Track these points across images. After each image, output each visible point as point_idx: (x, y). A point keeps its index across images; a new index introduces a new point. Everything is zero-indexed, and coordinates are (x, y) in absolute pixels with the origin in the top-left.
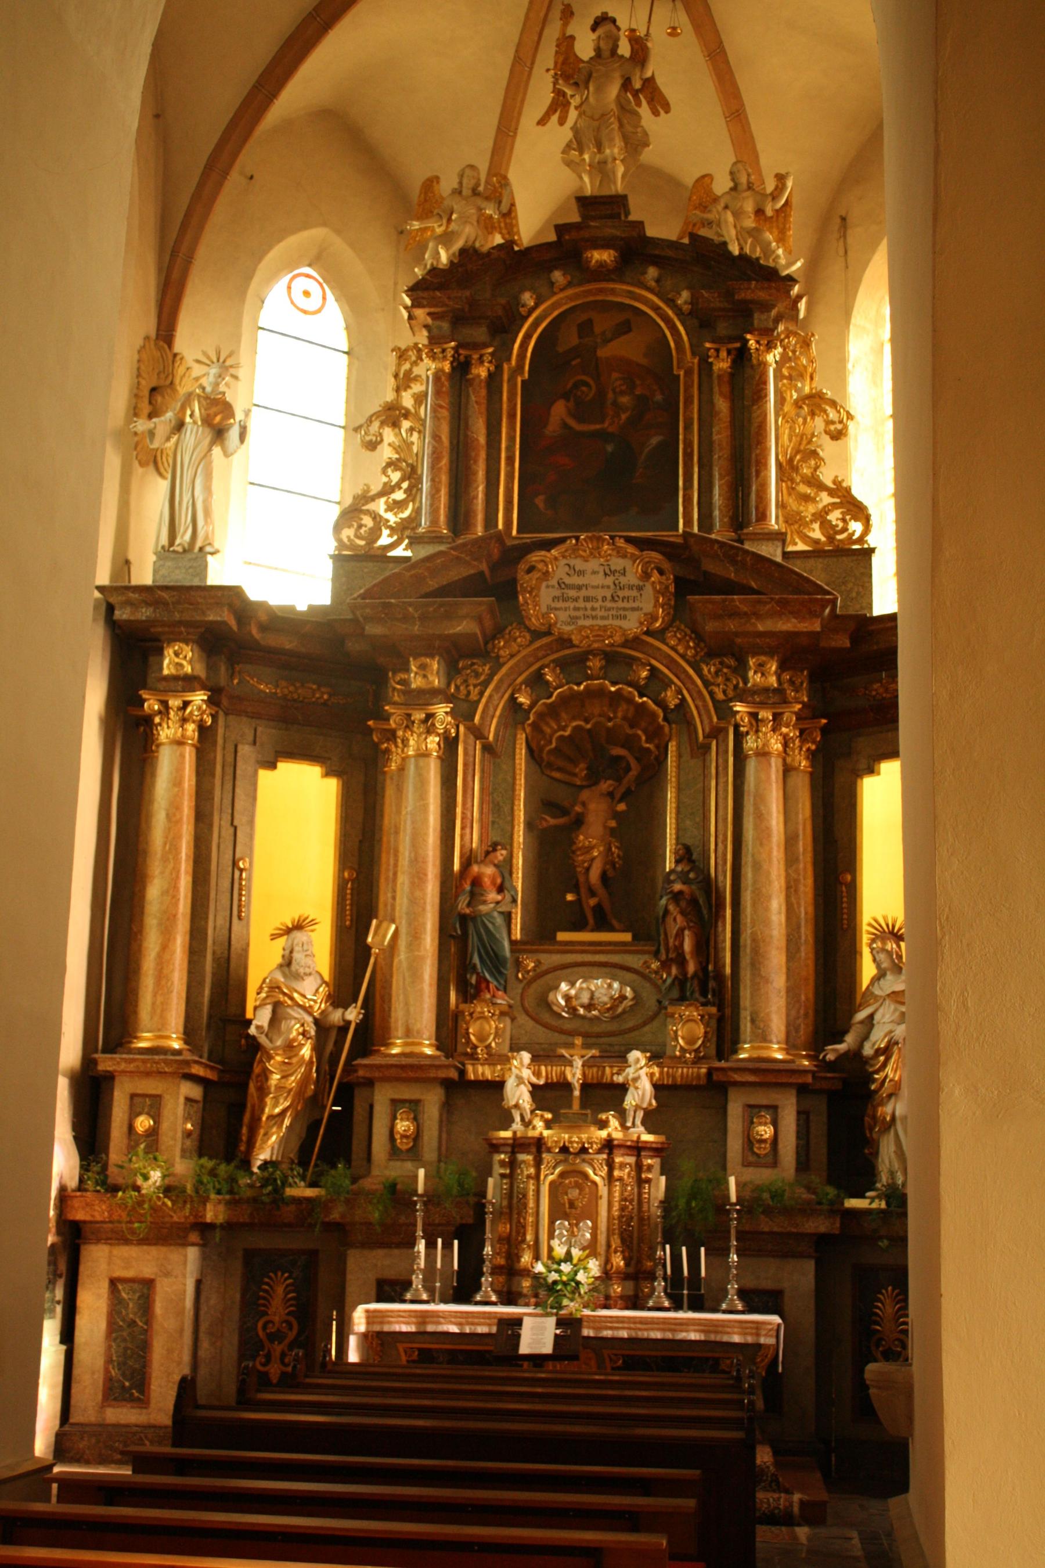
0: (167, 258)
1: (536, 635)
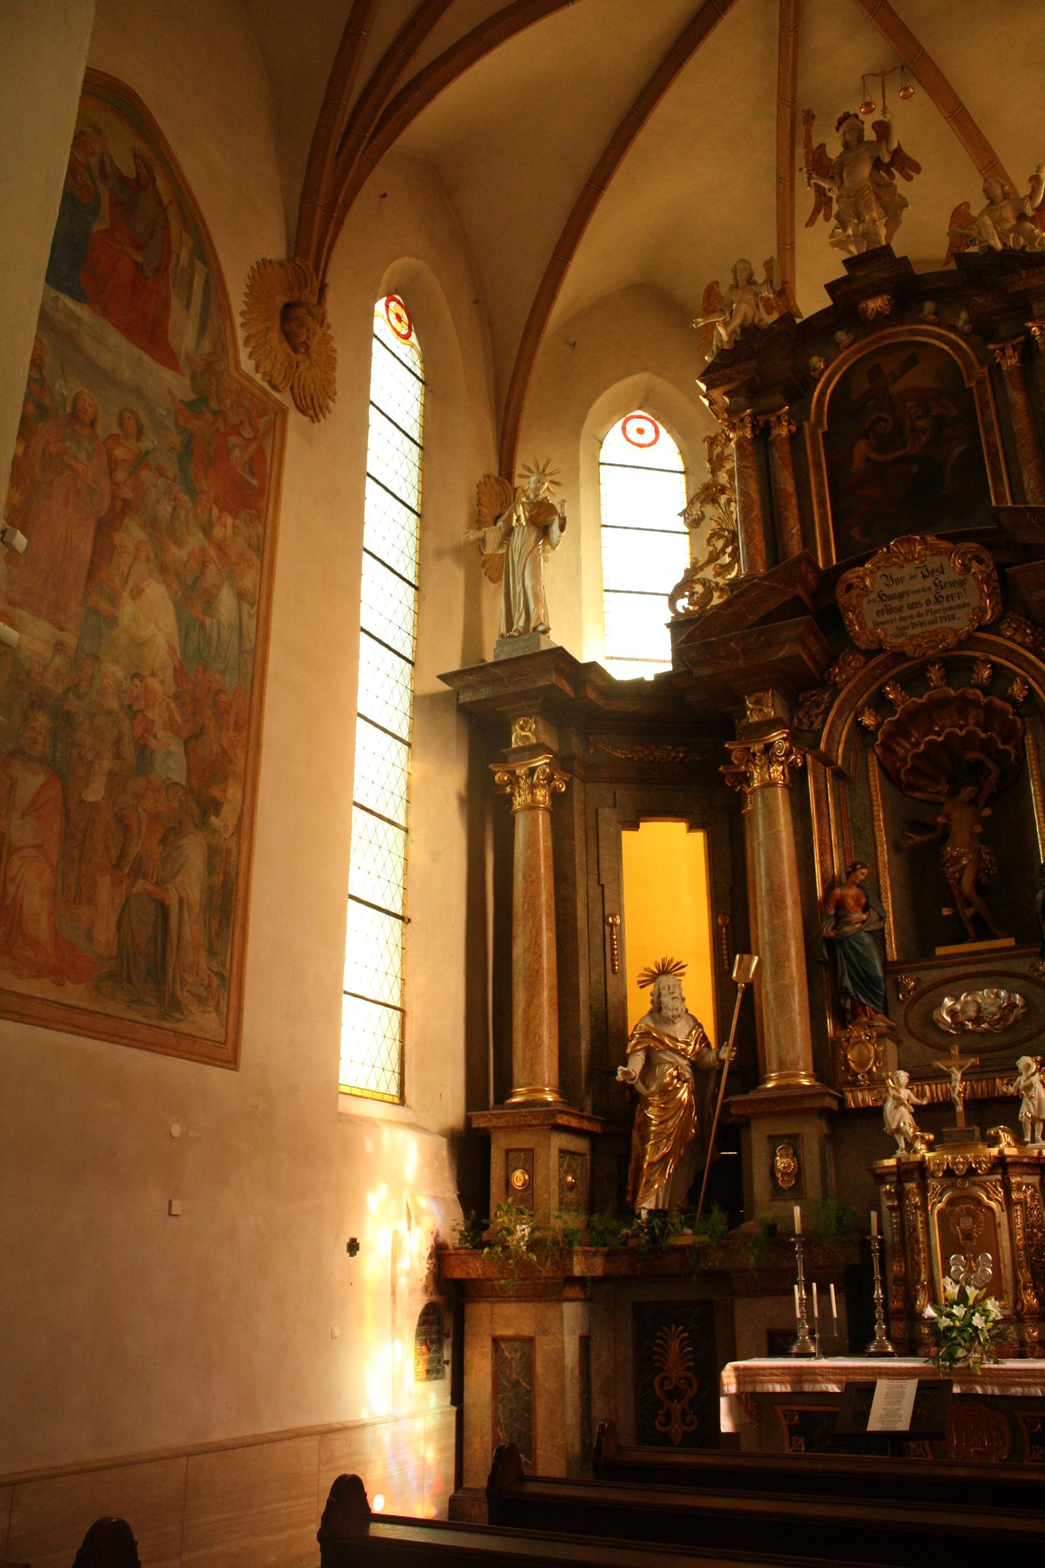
0: (503, 412)
1: (869, 654)
